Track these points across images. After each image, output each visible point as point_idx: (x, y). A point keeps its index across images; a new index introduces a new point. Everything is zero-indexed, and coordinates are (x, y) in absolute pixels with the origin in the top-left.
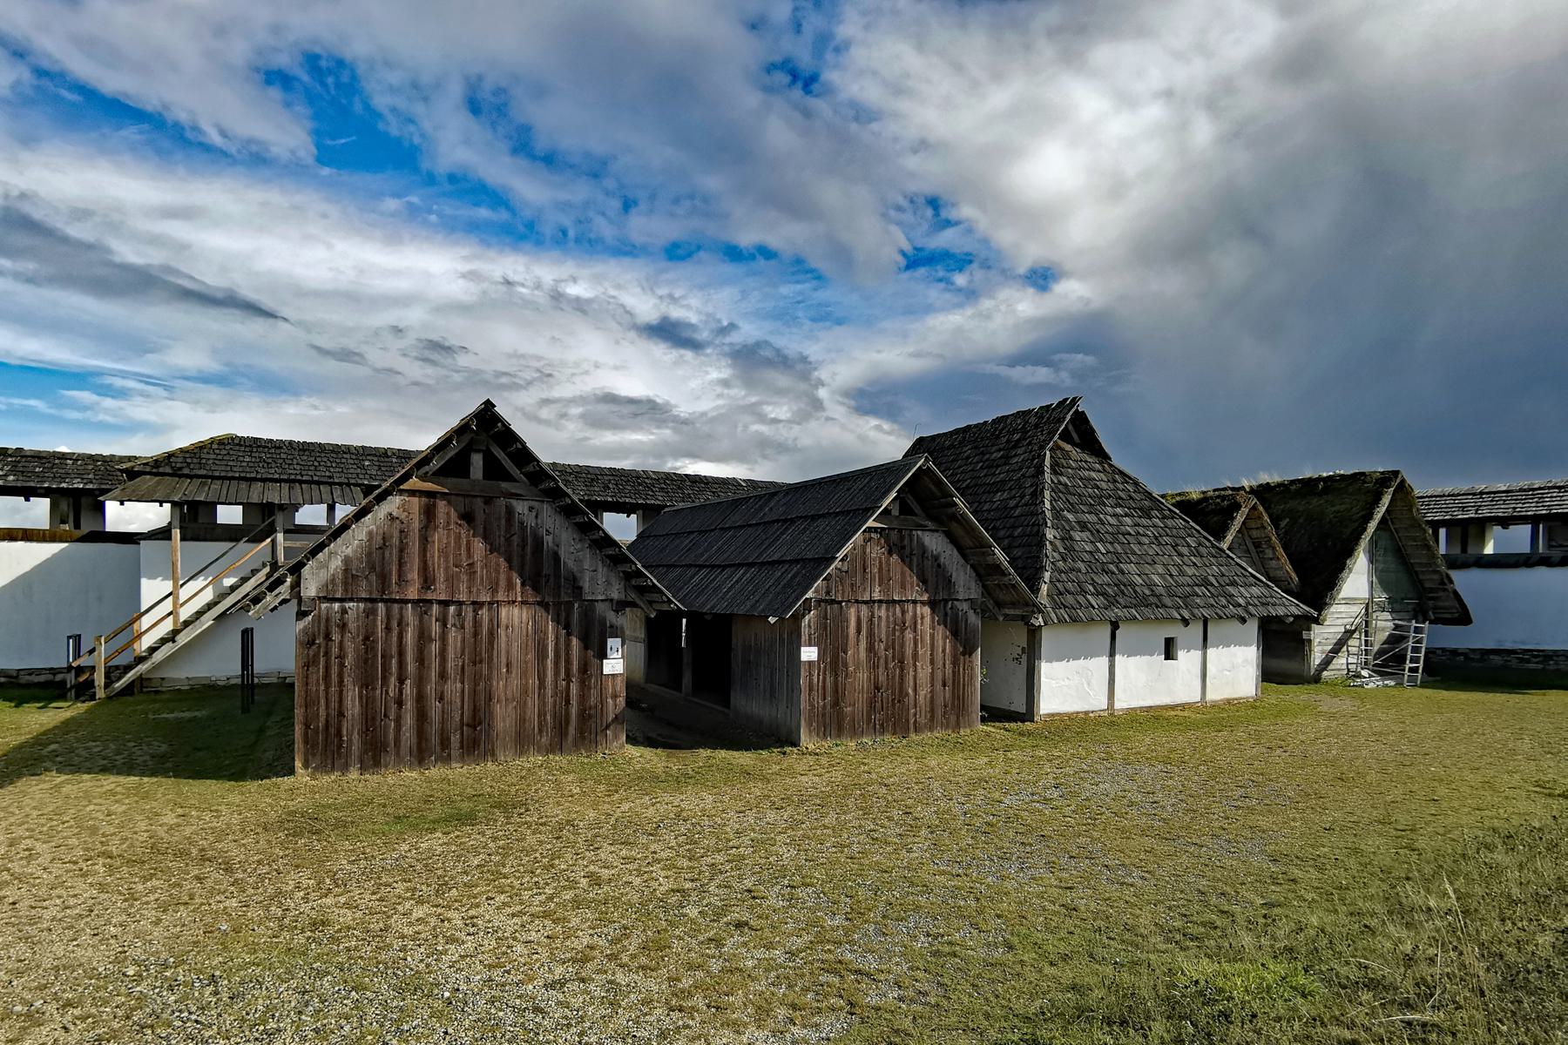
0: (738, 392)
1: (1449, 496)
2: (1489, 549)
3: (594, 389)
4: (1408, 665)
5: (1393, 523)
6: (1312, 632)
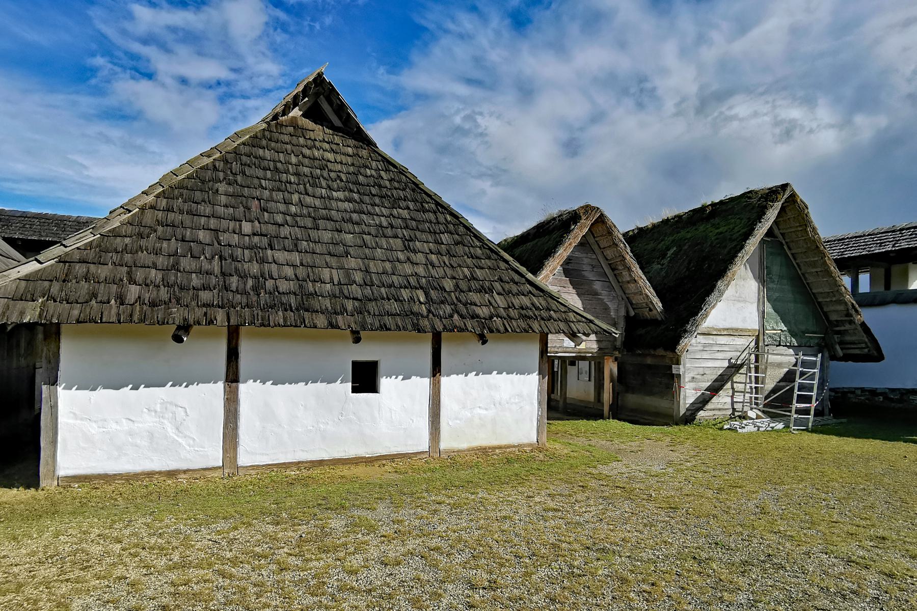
1: (868, 235)
4: (796, 405)
5: (790, 249)
6: (681, 366)
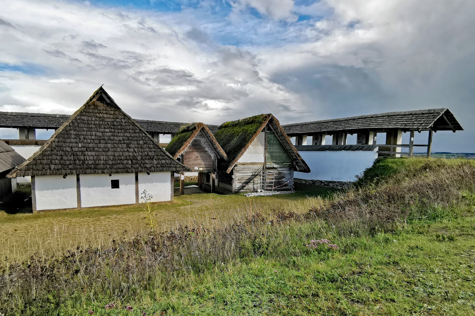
0: (221, 67)
2: (323, 143)
3: (159, 67)
